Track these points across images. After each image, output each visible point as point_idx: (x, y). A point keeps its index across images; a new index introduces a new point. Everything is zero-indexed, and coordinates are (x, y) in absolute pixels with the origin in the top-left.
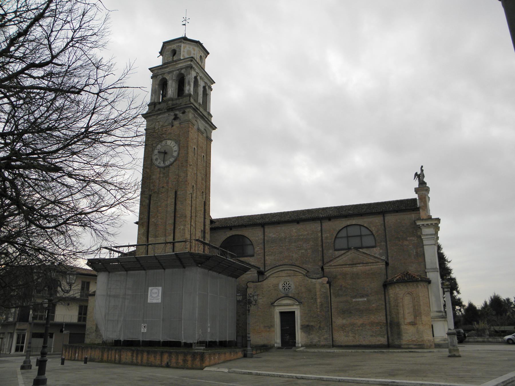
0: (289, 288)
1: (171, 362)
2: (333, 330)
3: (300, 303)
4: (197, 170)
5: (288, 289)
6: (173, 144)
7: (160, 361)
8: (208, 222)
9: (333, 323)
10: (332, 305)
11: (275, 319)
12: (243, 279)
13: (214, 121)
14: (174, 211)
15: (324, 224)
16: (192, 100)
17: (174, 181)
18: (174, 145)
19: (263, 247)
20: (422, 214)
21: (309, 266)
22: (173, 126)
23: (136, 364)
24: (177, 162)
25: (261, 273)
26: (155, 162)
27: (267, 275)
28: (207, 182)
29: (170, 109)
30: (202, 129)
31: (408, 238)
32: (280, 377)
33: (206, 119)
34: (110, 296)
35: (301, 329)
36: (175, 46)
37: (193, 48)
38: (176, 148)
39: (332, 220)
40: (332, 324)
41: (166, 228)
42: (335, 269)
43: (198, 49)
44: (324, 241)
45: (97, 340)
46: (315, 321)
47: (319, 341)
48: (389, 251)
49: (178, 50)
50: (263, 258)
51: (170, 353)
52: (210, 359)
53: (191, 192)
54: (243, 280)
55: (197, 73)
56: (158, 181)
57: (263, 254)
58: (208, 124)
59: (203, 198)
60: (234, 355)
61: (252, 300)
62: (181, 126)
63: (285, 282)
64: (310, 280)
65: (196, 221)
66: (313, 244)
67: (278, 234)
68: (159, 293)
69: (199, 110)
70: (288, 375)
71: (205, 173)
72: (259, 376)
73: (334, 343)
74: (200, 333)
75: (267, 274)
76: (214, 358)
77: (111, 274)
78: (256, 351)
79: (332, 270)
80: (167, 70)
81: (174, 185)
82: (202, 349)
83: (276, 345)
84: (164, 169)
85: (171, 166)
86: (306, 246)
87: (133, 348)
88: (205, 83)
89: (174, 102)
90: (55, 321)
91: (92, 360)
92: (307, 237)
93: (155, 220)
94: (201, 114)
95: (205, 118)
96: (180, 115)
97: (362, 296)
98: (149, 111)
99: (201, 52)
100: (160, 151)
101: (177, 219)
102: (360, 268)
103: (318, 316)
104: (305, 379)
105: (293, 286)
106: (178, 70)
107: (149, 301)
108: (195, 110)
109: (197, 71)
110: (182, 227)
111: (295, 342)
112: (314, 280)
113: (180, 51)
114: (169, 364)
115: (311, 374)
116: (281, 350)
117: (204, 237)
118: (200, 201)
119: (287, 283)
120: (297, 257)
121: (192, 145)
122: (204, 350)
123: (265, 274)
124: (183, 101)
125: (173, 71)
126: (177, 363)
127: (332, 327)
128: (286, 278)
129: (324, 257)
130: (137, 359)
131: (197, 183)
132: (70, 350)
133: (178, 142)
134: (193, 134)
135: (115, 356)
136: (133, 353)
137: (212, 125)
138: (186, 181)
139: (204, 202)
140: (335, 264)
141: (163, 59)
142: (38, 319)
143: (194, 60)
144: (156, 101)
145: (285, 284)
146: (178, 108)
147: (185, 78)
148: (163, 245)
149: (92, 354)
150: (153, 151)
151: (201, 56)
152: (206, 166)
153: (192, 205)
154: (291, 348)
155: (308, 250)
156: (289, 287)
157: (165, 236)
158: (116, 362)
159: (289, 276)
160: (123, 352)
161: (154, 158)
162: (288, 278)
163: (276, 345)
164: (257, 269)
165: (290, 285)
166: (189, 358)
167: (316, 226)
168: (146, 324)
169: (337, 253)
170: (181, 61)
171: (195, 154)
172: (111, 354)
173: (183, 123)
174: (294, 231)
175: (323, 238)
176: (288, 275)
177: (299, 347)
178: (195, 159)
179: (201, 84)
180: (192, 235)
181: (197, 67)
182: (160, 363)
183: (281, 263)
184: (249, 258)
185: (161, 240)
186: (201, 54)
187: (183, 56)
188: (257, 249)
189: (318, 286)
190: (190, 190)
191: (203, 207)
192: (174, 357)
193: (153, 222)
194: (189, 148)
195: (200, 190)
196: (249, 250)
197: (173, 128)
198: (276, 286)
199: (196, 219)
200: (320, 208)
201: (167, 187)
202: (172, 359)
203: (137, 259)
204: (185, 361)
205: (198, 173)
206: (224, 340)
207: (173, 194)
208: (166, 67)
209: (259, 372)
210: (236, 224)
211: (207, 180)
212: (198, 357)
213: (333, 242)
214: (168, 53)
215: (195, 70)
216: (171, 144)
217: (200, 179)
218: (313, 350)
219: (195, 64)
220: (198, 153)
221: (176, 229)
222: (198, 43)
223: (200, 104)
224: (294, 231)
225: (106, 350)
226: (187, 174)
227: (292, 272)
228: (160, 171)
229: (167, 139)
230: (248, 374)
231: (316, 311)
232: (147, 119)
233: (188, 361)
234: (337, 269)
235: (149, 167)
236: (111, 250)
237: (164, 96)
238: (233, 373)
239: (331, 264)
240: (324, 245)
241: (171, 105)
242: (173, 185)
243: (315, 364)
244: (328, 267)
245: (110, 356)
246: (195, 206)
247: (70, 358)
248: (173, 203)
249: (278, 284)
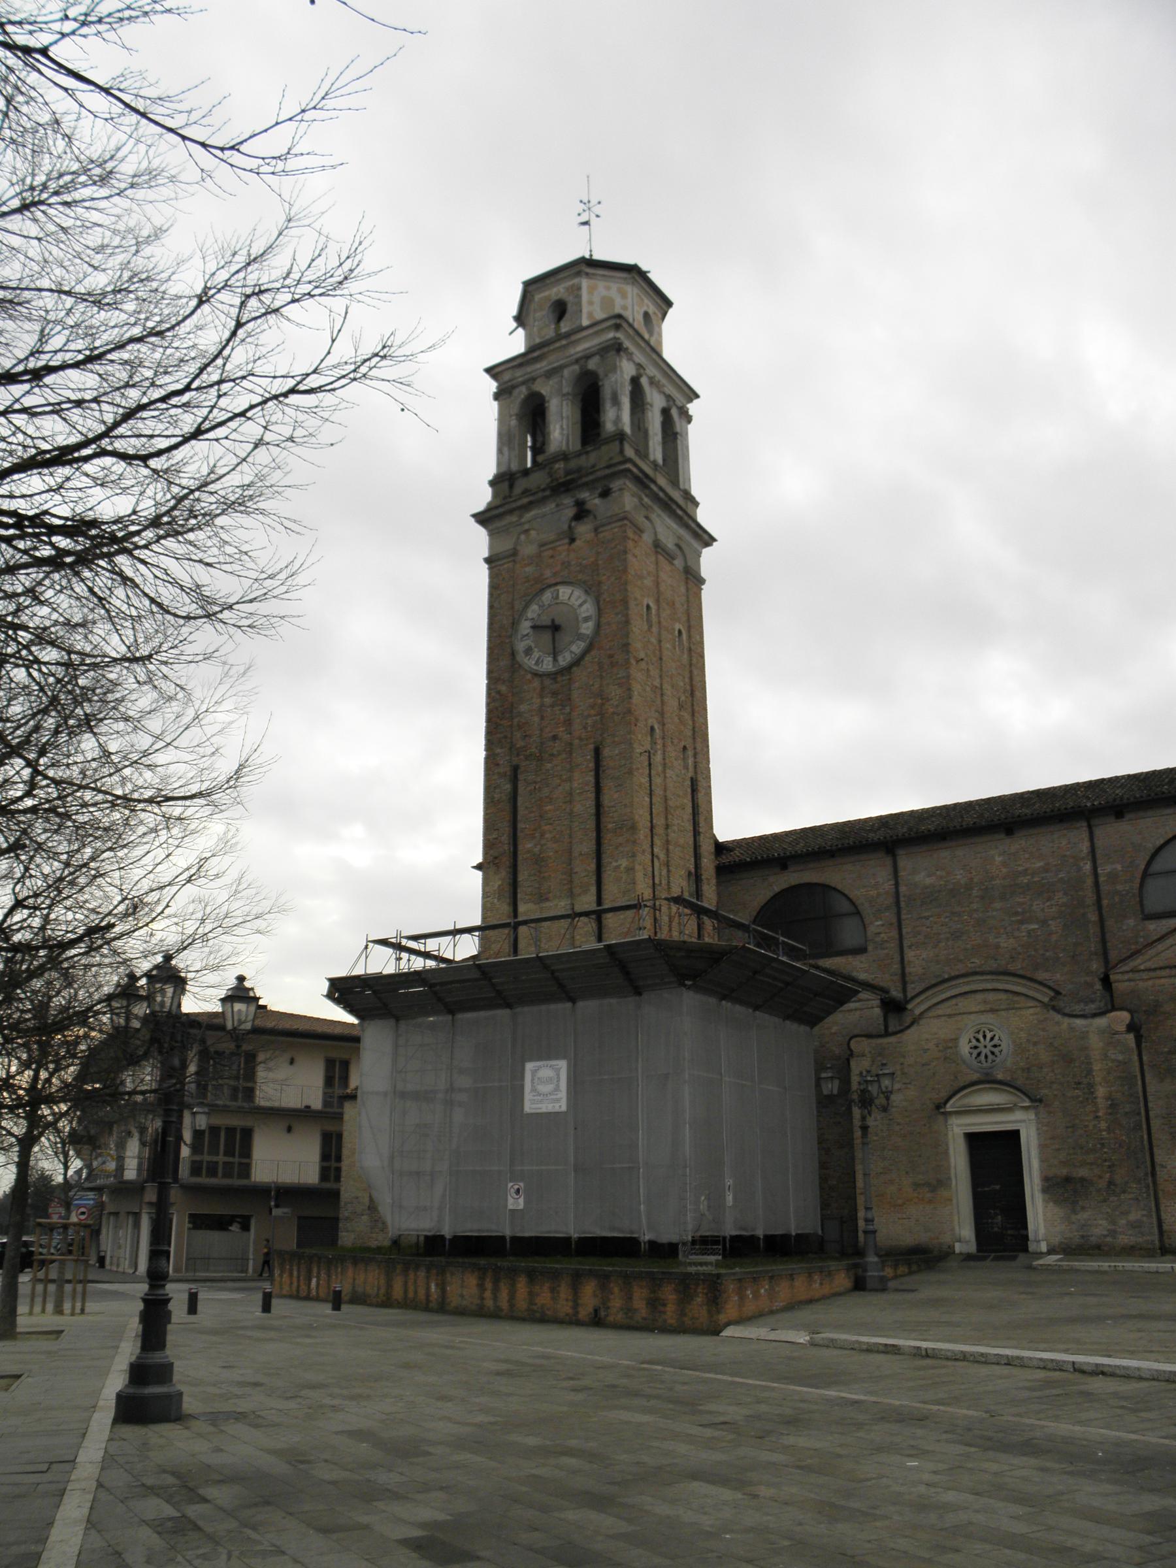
0: (993, 1053)
1: (608, 1308)
2: (1160, 1194)
3: (1037, 1101)
4: (661, 676)
5: (989, 1054)
6: (579, 597)
7: (570, 1304)
8: (707, 849)
9: (1158, 1168)
10: (1150, 1105)
11: (952, 1160)
12: (834, 1029)
13: (704, 516)
14: (593, 811)
15: (1098, 832)
16: (629, 452)
17: (589, 716)
18: (580, 601)
19: (894, 920)
21: (1057, 977)
22: (573, 540)
23: (495, 1315)
24: (594, 652)
25: (893, 1007)
26: (526, 660)
27: (917, 1012)
28: (696, 714)
29: (560, 488)
30: (669, 543)
32: (1007, 1364)
33: (680, 512)
34: (403, 1095)
35: (1045, 1190)
36: (562, 290)
37: (620, 291)
38: (588, 609)
39: (1128, 816)
40: (1153, 1174)
41: (571, 869)
42: (1150, 983)
43: (636, 291)
44: (1104, 888)
45: (374, 1235)
46: (1091, 1164)
47: (1113, 1233)
49: (570, 299)
50: (897, 958)
51: (604, 1279)
52: (742, 1298)
53: (644, 749)
54: (833, 1031)
55: (639, 366)
56: (536, 719)
57: (897, 942)
58: (687, 526)
59: (686, 767)
60: (821, 1284)
61: (875, 1094)
62: (601, 535)
63: (978, 1032)
64: (1067, 1020)
65: (668, 842)
66: (1065, 900)
67: (944, 873)
68: (558, 1081)
69: (654, 482)
70: (1041, 1359)
71: (688, 687)
72: (929, 1362)
73: (1167, 1241)
74: (703, 1207)
75: (916, 1007)
76: (756, 1296)
77: (403, 1025)
78: (896, 1267)
79: (1141, 984)
80: (542, 366)
81: (589, 729)
82: (710, 1264)
83: (958, 1248)
84: (555, 679)
85: (575, 669)
86: (1043, 910)
87: (482, 1262)
88: (669, 398)
89: (573, 464)
90: (253, 1179)
91: (359, 1299)
92: (1043, 879)
93: (536, 845)
94: (661, 494)
95: (674, 507)
96: (594, 502)
98: (498, 502)
99: (646, 301)
100: (538, 623)
101: (607, 837)
103: (1103, 1145)
104: (1113, 1375)
105: (1006, 1045)
106: (577, 361)
107: (529, 1107)
108: (643, 481)
109: (637, 360)
110: (624, 863)
111: (1026, 1238)
112: (1079, 1022)
113: (579, 304)
114: (603, 1314)
115: (1132, 1354)
116: (979, 1264)
117: (698, 894)
118: (677, 776)
119: (985, 1037)
120: (1015, 949)
121: (641, 598)
122: (717, 1265)
123: (909, 1006)
124: (598, 458)
125: (561, 368)
126: (629, 1310)
127: (1155, 1183)
128: (984, 1018)
129: (1109, 944)
130: (495, 1298)
131: (663, 717)
132: (295, 1268)
133: (592, 589)
134: (640, 560)
135: (428, 1289)
136: (482, 1279)
137: (700, 532)
138: (629, 712)
139: (692, 778)
140: (1149, 965)
141: (528, 337)
142: (204, 1172)
143: (625, 325)
144: (514, 467)
145: (978, 1040)
146: (585, 480)
147: (600, 383)
148: (564, 923)
149: (357, 1282)
150: (515, 624)
151: (646, 315)
152: (691, 665)
153: (651, 790)
154: (1014, 1258)
155: (1050, 922)
156: (993, 1049)
157: (571, 895)
158: (431, 1305)
159: (992, 1011)
160: (452, 1274)
161: (521, 646)
162: (989, 1018)
163: (958, 1248)
164: (880, 993)
165: (996, 1041)
166: (669, 1294)
168: (522, 1184)
169: (1155, 928)
170: (584, 333)
171: (650, 626)
172: (415, 1281)
173: (606, 528)
174: (998, 859)
175: (1101, 879)
176: (988, 1007)
177: (1042, 1253)
178: (653, 640)
179: (656, 401)
180: (658, 888)
181: (638, 346)
182: (570, 1311)
183: (960, 968)
184: (850, 958)
185: (560, 906)
186: (645, 308)
187: (590, 315)
188: (876, 926)
189: (1096, 1043)
190: (642, 742)
191: (689, 797)
192: (616, 1290)
193: (528, 852)
194: (632, 604)
195: (676, 741)
196: (848, 933)
197: (574, 546)
199: (667, 835)
200: (1078, 784)
201: (566, 737)
202: (612, 1297)
203: (483, 973)
204: (654, 1304)
205: (666, 686)
206: (780, 1231)
207: (590, 756)
208: (538, 357)
209: (924, 1345)
210: (800, 847)
211: (696, 708)
212: (699, 1290)
213: (1136, 891)
214: (541, 315)
215: (630, 357)
216: (573, 599)
217: (672, 704)
218: (1093, 1265)
219: (628, 336)
220: (659, 622)
221: (603, 869)
222: (634, 273)
223: (655, 464)
224: (998, 859)
225: (399, 1267)
226: (629, 689)
227: (1003, 996)
228: (543, 689)
230: (883, 1352)
231: (1095, 1126)
232: (490, 528)
233: (665, 1305)
234: (1158, 982)
235: (506, 676)
236: (399, 947)
237: (537, 450)
238: (828, 1347)
239: (1139, 961)
240: (1105, 902)
241: (562, 473)
242: (585, 728)
243: (1129, 1317)
244: (1126, 977)
245: (411, 1289)
246: (661, 793)
247: (295, 1293)
248: (591, 788)
249: (955, 1040)
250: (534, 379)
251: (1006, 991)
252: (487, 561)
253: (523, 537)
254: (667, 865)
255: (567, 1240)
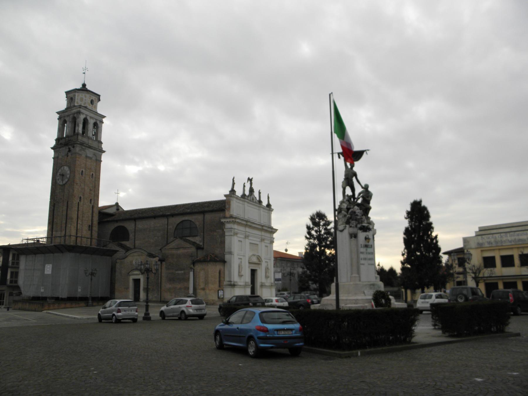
20: (227, 214)
31: (217, 231)
38: (68, 172)
48: (205, 239)
49: (73, 98)
80: (66, 114)
96: (72, 148)
97: (181, 270)
102: (181, 251)
106: (72, 114)
140: (168, 248)
150: (57, 173)
167: (164, 221)
175: (168, 229)
179: (91, 122)
186: (92, 98)
187: (77, 103)
198: (132, 262)
229: (64, 166)
248: (66, 210)
250: (65, 117)
251: (141, 252)
252: (53, 158)
253: (60, 154)
254: (82, 225)
255: (98, 297)
